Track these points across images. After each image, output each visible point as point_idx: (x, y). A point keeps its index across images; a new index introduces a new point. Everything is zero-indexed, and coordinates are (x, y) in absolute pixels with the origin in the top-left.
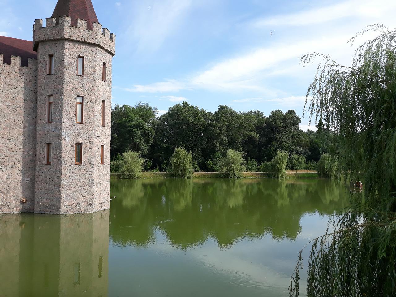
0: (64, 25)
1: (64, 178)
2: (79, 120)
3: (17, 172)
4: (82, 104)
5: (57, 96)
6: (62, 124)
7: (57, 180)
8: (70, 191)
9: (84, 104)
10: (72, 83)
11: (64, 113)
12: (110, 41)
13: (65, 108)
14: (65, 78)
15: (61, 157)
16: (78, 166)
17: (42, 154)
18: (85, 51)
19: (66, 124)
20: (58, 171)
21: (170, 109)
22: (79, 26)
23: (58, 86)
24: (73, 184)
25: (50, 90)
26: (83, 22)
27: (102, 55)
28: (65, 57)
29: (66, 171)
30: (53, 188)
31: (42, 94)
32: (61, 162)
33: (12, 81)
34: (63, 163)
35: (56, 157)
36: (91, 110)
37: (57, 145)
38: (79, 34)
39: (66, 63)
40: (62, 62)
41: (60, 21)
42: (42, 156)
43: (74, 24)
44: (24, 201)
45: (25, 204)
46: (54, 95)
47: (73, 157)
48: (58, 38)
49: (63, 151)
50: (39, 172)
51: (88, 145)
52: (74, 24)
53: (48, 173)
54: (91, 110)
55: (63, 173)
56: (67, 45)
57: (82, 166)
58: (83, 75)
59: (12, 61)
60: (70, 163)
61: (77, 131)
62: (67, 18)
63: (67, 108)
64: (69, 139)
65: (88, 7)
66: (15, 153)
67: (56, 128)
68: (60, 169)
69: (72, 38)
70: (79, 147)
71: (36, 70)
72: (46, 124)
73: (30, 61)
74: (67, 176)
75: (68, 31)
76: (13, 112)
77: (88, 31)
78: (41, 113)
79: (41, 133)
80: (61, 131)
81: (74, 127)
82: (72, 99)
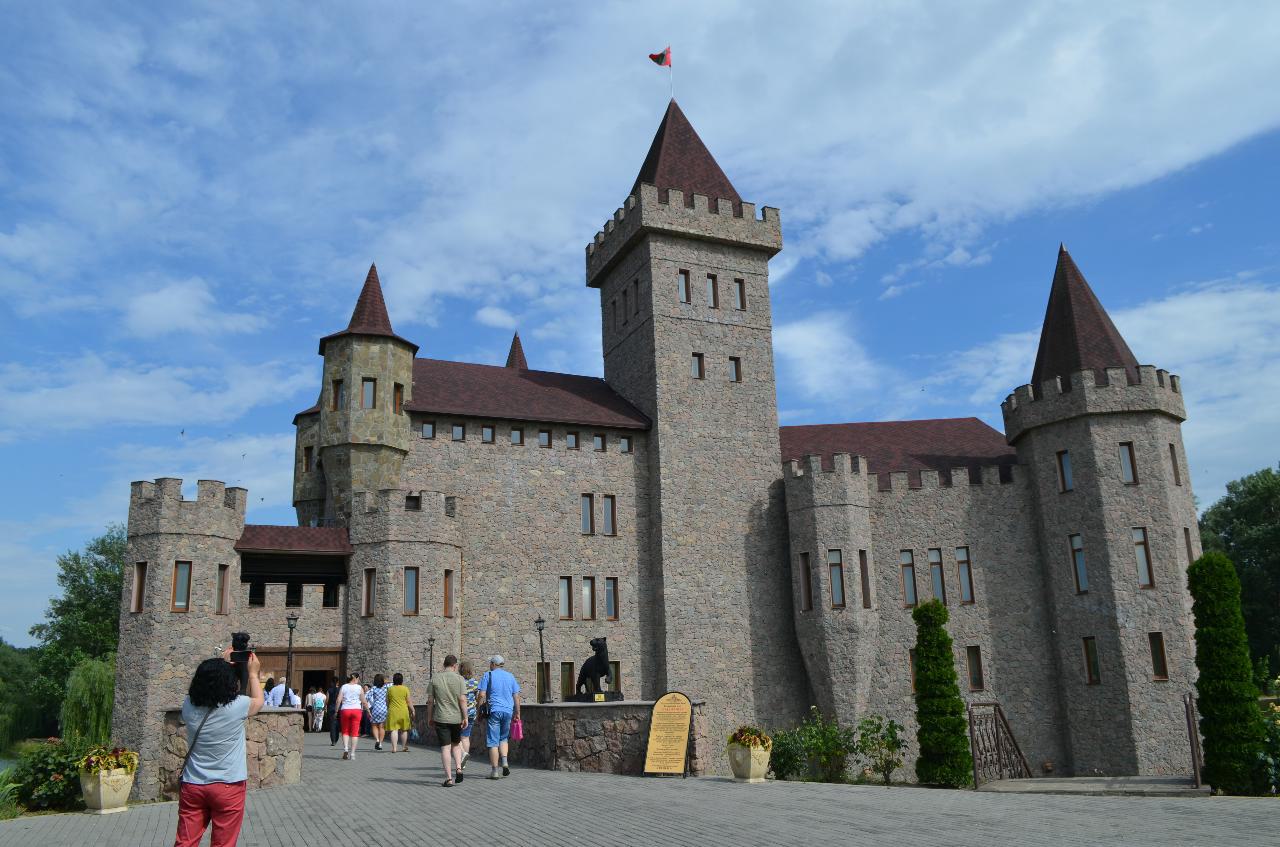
0: (1082, 388)
1: (1137, 713)
2: (1146, 581)
3: (1025, 704)
4: (1145, 543)
5: (1090, 534)
6: (1113, 593)
7: (1121, 717)
8: (1153, 740)
9: (1150, 543)
10: (1118, 503)
11: (1113, 570)
12: (1174, 394)
13: (1114, 558)
14: (1103, 494)
15: (1122, 665)
16: (1161, 684)
17: (1075, 663)
18: (1134, 432)
19: (1122, 593)
20: (1120, 698)
21: (1231, 488)
22: (1111, 381)
23: (1090, 513)
24: (1158, 726)
25: (1073, 523)
26: (1118, 371)
27: (1165, 430)
28: (1096, 452)
29: (1138, 696)
30: (1114, 736)
31: (1055, 535)
32: (1124, 677)
33: (990, 518)
34: (1129, 678)
35: (1110, 667)
36: (1167, 555)
37: (1108, 640)
38: (1116, 398)
39: (1100, 464)
40: (1090, 462)
41: (1074, 381)
42: (1076, 668)
43: (1102, 382)
44: (1050, 768)
45: (494, 782)
46: (1083, 534)
47: (1146, 663)
48: (1074, 415)
49: (1124, 653)
50: (1074, 702)
51: (1175, 634)
52: (1102, 382)
53: (1097, 703)
54: (1167, 555)
55: (1131, 700)
56: (1095, 429)
57: (1170, 684)
58: (1136, 482)
59: (985, 477)
60: (1144, 679)
61: (1146, 607)
62: (1087, 373)
63: (1117, 559)
64: (1132, 624)
65: (1111, 334)
66: (1016, 664)
67: (1100, 603)
68: (1125, 693)
69: (1104, 411)
70: (1156, 639)
71: (1031, 485)
72: (1076, 598)
73: (1015, 471)
74: (1142, 707)
75: (1095, 400)
76: (1000, 580)
77: (1130, 388)
78: (1059, 574)
79: (1066, 616)
80: (1115, 609)
81: (1139, 598)
82: (1124, 538)
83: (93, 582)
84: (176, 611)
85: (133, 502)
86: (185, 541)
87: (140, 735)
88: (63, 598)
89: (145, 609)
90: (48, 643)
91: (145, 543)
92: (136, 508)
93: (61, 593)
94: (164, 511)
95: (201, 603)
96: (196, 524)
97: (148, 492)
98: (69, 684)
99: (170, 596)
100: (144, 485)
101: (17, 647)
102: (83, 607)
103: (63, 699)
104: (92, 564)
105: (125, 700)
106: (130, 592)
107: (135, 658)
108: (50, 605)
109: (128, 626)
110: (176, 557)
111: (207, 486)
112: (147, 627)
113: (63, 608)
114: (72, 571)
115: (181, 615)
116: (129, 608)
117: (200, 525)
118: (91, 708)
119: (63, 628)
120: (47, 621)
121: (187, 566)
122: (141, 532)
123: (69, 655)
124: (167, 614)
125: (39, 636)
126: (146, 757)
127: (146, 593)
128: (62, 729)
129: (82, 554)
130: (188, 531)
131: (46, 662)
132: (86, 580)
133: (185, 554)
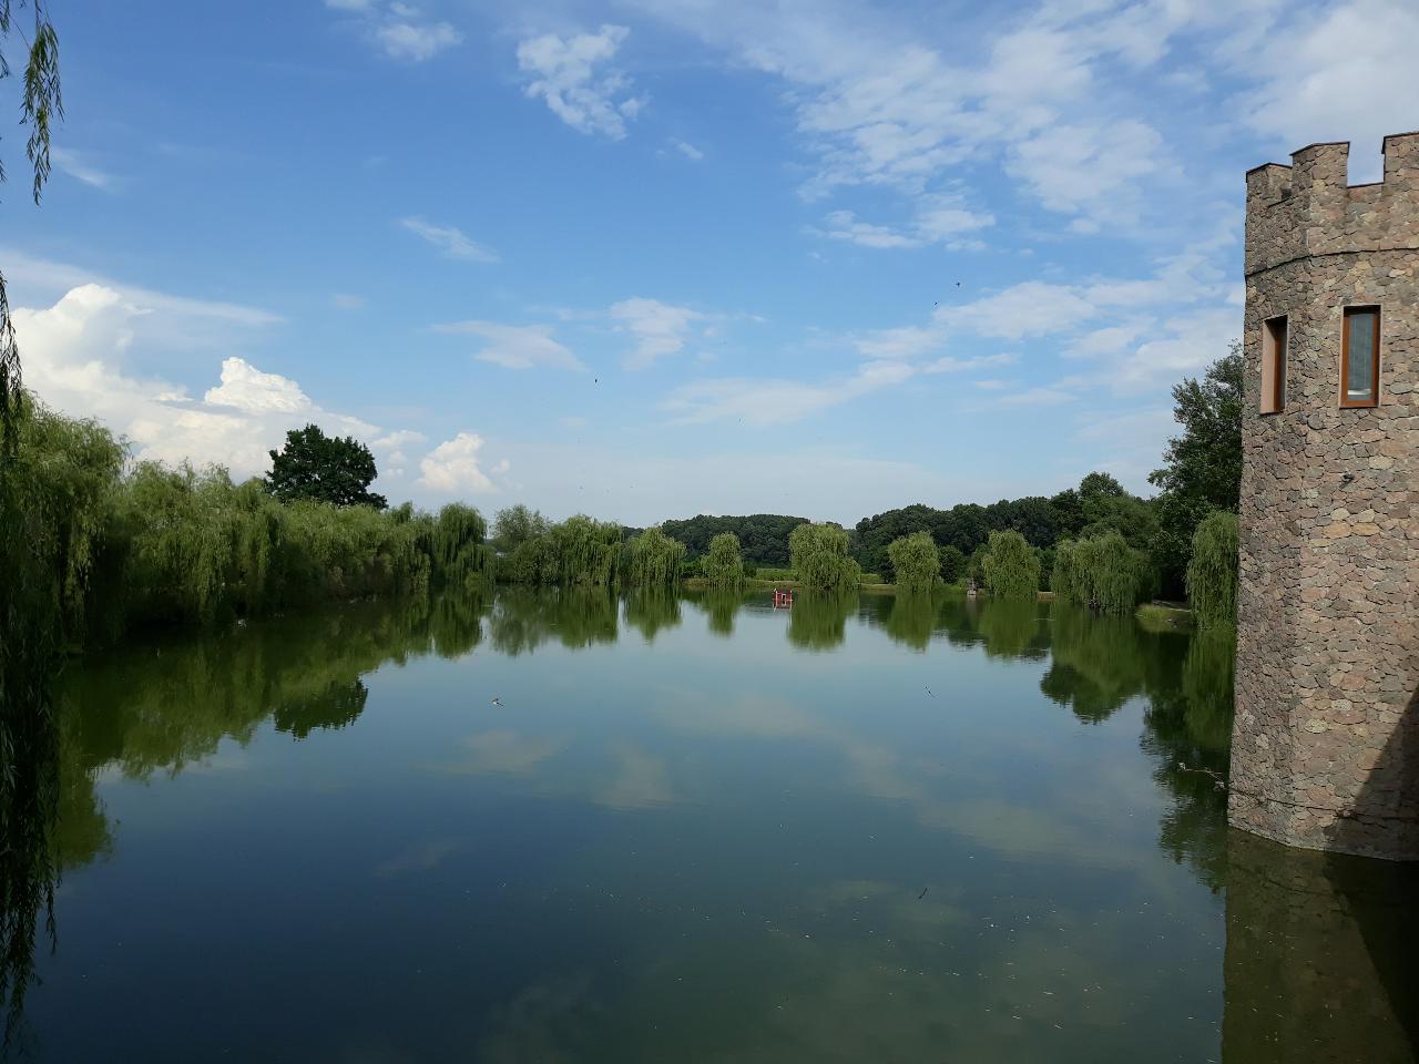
83: (1217, 416)
84: (1349, 406)
85: (1251, 210)
86: (1362, 266)
87: (1291, 642)
88: (1183, 438)
89: (1289, 405)
90: (1170, 491)
91: (1281, 280)
92: (1259, 219)
93: (1181, 431)
94: (1315, 212)
95: (1403, 387)
96: (1385, 228)
97: (1276, 180)
98: (1195, 540)
99: (1337, 378)
100: (1270, 171)
101: (984, 504)
102: (1206, 447)
103: (1190, 557)
104: (1214, 395)
105: (1260, 573)
106: (1258, 376)
107: (1273, 498)
108: (1169, 447)
109: (1259, 440)
110: (1347, 300)
111: (1405, 148)
112: (1294, 442)
113: (1183, 450)
114: (1191, 402)
115: (1362, 413)
116: (1257, 407)
117: (1393, 230)
118: (1223, 571)
119: (1185, 474)
120: (1167, 466)
121: (1369, 319)
122: (1272, 261)
123: (1194, 506)
124: (1333, 412)
125: (1159, 484)
126: (1304, 683)
127: (1288, 376)
128: (1189, 594)
129: (1201, 382)
130: (1368, 245)
131: (1166, 513)
132: (1209, 414)
133: (1364, 292)
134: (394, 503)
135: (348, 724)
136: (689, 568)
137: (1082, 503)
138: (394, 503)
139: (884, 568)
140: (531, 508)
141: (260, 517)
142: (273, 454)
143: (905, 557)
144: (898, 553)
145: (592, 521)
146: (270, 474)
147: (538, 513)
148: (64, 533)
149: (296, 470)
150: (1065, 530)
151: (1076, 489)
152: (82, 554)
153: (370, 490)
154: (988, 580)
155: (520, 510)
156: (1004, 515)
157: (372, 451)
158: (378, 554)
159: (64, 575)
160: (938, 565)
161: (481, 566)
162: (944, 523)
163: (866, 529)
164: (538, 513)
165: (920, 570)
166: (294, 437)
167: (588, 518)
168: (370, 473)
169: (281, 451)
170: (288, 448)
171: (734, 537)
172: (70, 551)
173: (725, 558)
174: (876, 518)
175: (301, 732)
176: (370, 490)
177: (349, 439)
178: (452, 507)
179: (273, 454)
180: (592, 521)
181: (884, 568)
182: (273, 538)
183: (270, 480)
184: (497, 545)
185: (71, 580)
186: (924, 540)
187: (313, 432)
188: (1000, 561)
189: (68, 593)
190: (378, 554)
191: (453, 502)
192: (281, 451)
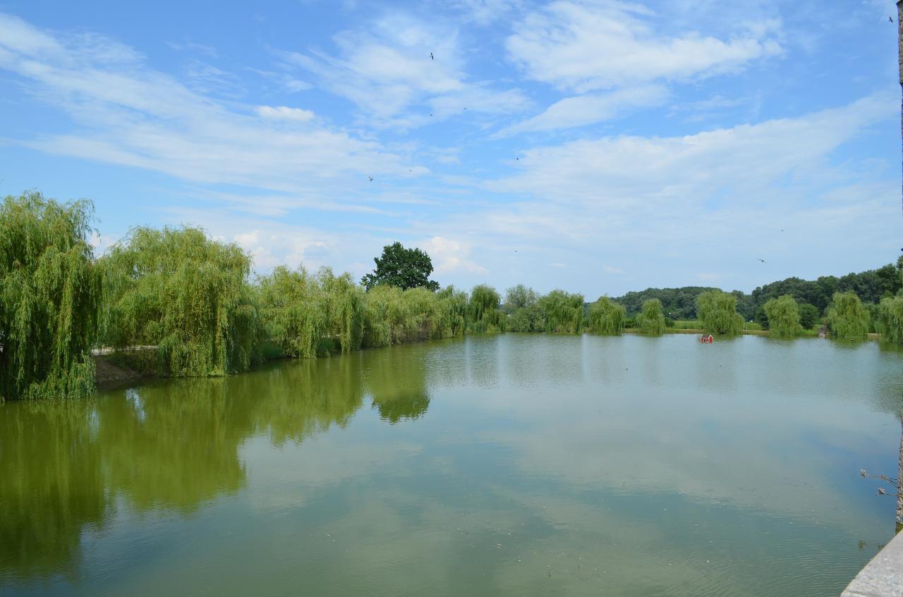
134: (443, 286)
135: (334, 426)
136: (629, 322)
137: (899, 273)
138: (443, 286)
139: (762, 320)
140: (527, 286)
141: (346, 299)
142: (376, 260)
143: (775, 312)
144: (770, 309)
145: (565, 293)
146: (375, 272)
147: (531, 290)
148: (214, 308)
149: (389, 269)
150: (887, 291)
151: (895, 263)
152: (223, 319)
153: (429, 279)
154: (834, 327)
155: (520, 287)
156: (850, 283)
157: (430, 256)
158: (428, 316)
159: (215, 331)
160: (798, 317)
161: (497, 323)
162: (811, 289)
163: (758, 294)
164: (531, 290)
165: (786, 320)
166: (387, 250)
167: (562, 292)
168: (429, 268)
169: (380, 258)
170: (384, 256)
171: (658, 301)
172: (218, 317)
173: (652, 315)
174: (765, 287)
175: (394, 419)
176: (429, 279)
177: (417, 249)
178: (479, 287)
179: (376, 260)
180: (565, 293)
181: (762, 320)
182: (354, 306)
183: (375, 275)
184: (508, 310)
185: (218, 334)
186: (788, 300)
187: (397, 246)
188: (841, 313)
189: (217, 341)
190: (428, 316)
191: (480, 284)
192: (380, 258)
